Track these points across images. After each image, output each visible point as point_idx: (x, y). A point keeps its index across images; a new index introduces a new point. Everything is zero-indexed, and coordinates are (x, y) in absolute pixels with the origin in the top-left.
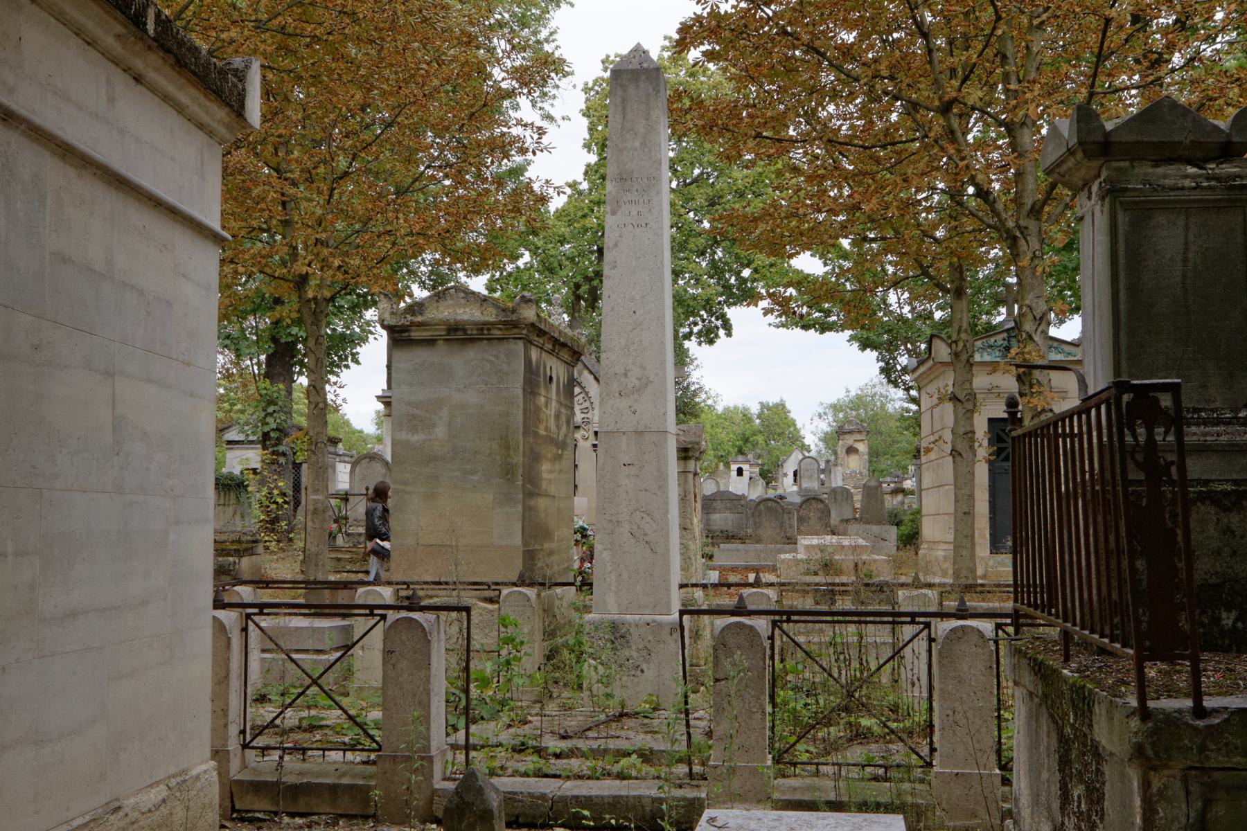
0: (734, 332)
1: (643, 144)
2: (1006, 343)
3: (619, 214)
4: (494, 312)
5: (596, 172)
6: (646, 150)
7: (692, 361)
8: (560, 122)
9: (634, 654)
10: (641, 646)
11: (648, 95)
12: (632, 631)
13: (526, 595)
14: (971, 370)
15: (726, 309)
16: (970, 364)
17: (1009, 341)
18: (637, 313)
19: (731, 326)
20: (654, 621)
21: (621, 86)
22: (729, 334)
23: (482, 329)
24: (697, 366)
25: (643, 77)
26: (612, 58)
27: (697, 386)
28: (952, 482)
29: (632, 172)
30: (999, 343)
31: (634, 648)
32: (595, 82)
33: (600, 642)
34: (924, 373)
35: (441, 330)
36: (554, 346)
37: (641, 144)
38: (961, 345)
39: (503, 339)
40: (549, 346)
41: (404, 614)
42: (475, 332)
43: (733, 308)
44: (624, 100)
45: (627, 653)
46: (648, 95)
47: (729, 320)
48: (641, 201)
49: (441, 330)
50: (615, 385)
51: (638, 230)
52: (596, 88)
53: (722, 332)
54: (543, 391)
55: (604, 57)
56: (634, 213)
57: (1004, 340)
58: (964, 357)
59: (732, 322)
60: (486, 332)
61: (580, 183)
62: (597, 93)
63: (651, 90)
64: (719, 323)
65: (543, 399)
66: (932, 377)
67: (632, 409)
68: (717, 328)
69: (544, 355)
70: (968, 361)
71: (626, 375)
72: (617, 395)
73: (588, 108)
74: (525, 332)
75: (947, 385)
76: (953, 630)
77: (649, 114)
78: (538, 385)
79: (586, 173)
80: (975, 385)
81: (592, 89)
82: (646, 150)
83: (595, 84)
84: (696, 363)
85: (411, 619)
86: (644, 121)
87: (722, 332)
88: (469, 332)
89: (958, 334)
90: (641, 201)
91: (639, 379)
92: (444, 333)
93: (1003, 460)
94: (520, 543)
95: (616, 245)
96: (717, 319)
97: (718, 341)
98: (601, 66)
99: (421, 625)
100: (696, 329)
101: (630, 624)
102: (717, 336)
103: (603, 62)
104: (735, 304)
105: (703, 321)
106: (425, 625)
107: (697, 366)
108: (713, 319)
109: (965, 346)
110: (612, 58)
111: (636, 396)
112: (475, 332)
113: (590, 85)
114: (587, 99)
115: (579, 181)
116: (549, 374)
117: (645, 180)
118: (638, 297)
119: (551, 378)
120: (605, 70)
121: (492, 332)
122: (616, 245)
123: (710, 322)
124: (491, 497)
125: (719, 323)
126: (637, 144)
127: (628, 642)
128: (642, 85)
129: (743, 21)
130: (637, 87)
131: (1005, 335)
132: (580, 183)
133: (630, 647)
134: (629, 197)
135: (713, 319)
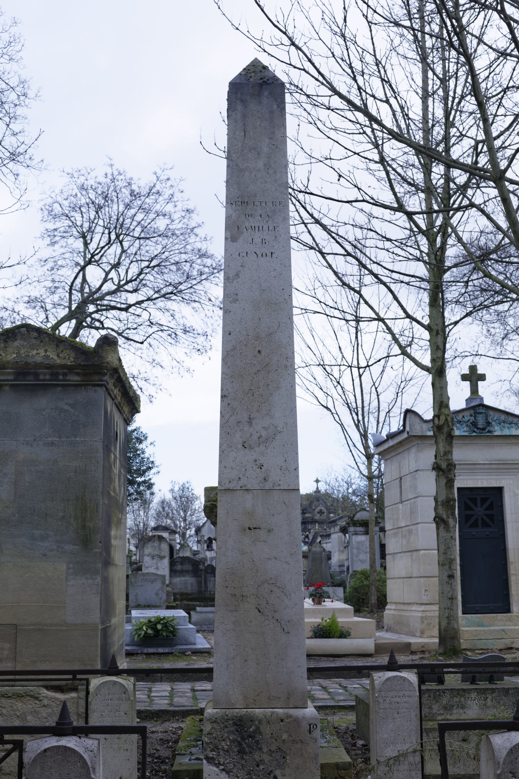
1: (267, 166)
2: (472, 418)
3: (240, 240)
4: (73, 355)
6: (271, 171)
9: (266, 758)
10: (274, 748)
12: (262, 729)
13: (122, 685)
14: (452, 442)
16: (450, 438)
17: (475, 417)
18: (263, 353)
20: (289, 716)
23: (57, 374)
28: (436, 548)
29: (255, 196)
30: (466, 419)
31: (265, 750)
33: (223, 743)
35: (9, 374)
39: (81, 385)
41: (52, 742)
42: (48, 377)
45: (257, 756)
46: (272, 112)
48: (266, 227)
49: (9, 374)
54: (113, 449)
56: (258, 240)
58: (445, 430)
60: (61, 377)
66: (401, 450)
72: (240, 446)
76: (388, 679)
77: (273, 133)
82: (271, 171)
84: (149, 441)
85: (66, 749)
88: (41, 377)
90: (266, 227)
92: (11, 377)
93: (471, 526)
94: (98, 621)
95: (237, 275)
99: (81, 757)
101: (260, 721)
106: (85, 756)
109: (446, 420)
111: (262, 448)
112: (48, 377)
117: (271, 204)
121: (68, 378)
122: (237, 275)
124: (64, 567)
126: (260, 164)
127: (257, 742)
128: (265, 101)
130: (260, 103)
133: (260, 749)
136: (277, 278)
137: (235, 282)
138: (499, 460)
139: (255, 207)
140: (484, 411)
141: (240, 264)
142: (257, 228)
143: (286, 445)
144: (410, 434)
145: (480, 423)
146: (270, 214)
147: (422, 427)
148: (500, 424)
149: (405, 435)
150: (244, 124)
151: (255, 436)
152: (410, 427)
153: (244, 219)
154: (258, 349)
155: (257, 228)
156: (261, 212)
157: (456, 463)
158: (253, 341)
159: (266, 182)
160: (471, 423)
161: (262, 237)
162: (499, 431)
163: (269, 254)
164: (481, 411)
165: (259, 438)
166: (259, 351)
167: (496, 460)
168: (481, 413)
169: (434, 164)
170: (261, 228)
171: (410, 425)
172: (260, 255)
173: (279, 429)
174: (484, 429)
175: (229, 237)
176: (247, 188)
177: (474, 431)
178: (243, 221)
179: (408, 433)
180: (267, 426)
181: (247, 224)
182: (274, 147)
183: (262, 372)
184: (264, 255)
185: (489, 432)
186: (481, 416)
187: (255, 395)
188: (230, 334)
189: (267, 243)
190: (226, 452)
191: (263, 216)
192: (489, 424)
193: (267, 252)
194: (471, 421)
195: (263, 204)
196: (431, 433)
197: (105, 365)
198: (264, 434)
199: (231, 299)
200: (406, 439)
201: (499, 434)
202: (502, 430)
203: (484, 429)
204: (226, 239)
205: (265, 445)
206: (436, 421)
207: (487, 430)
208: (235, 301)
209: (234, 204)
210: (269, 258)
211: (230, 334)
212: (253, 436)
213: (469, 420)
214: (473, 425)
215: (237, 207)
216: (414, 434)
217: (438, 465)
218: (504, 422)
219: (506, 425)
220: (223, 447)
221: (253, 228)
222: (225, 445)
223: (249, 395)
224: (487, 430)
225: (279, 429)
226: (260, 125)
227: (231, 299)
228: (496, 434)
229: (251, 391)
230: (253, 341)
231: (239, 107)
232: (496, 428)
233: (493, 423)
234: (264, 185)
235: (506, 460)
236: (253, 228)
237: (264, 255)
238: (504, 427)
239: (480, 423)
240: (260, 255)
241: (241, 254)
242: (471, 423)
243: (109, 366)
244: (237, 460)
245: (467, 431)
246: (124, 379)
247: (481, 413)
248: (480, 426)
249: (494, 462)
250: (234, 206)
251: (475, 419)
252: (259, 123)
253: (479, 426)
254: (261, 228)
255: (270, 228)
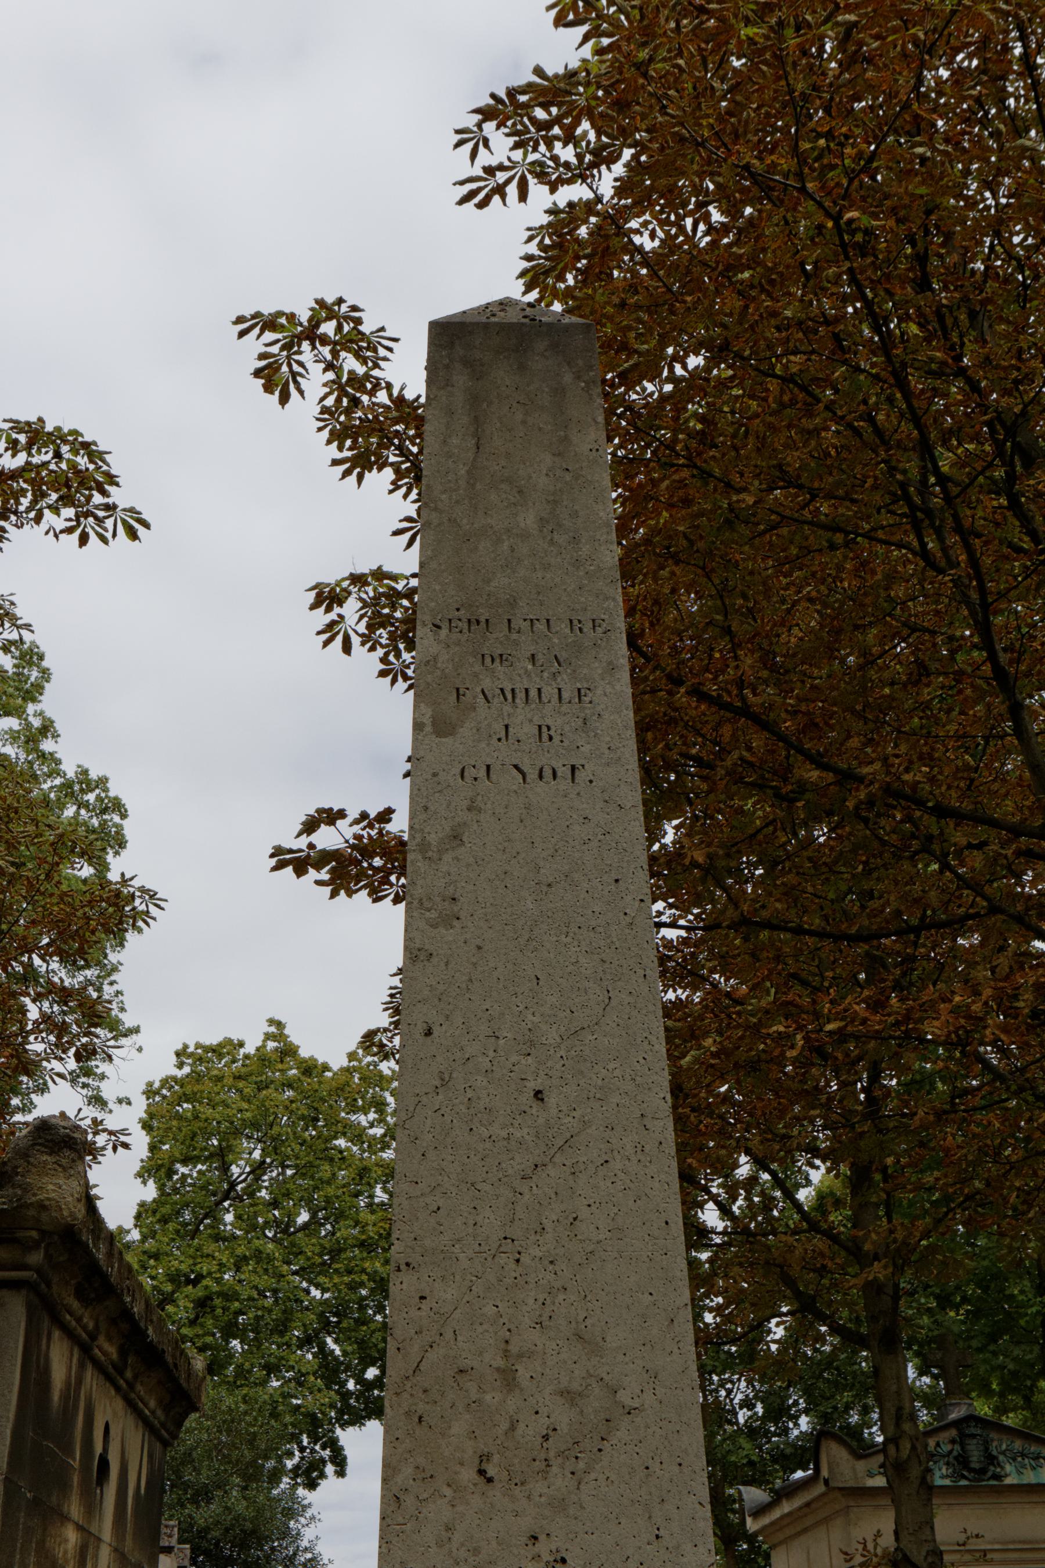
0: (349, 1470)
2: (957, 1447)
3: (466, 731)
5: (154, 1212)
6: (561, 539)
7: (305, 1508)
8: (111, 1105)
11: (559, 391)
14: (930, 1500)
15: (338, 1431)
18: (552, 1100)
19: (345, 1458)
21: (467, 363)
22: (341, 1473)
24: (313, 1518)
25: (541, 345)
26: (191, 1049)
27: (309, 1556)
29: (513, 603)
30: (946, 1448)
32: (165, 1082)
34: (790, 1514)
36: (123, 1352)
37: (542, 521)
38: (906, 1446)
40: (108, 1349)
43: (350, 1430)
44: (474, 400)
46: (559, 391)
47: (342, 1448)
48: (549, 692)
50: (458, 1428)
51: (541, 791)
52: (164, 1092)
53: (330, 1469)
54: (75, 1509)
55: (180, 1047)
56: (524, 730)
57: (953, 1442)
58: (915, 1472)
59: (346, 1452)
61: (128, 1232)
62: (164, 1097)
63: (568, 378)
64: (327, 1453)
65: (72, 1536)
66: (809, 1521)
67: (542, 1537)
68: (323, 1462)
69: (91, 1378)
70: (923, 1480)
71: (508, 1379)
72: (468, 1475)
73: (151, 1115)
74: (36, 1258)
75: (878, 1534)
78: (64, 1487)
79: (138, 1217)
80: (939, 1538)
81: (157, 1092)
83: (162, 1087)
84: (309, 1513)
86: (548, 459)
87: (330, 1469)
89: (898, 1425)
90: (549, 692)
91: (569, 1396)
95: (456, 837)
96: (323, 1448)
97: (323, 1484)
98: (174, 1059)
100: (289, 1464)
102: (322, 1475)
103: (178, 1054)
104: (352, 1423)
105: (302, 1449)
107: (313, 1518)
108: (317, 1448)
109: (914, 1448)
110: (191, 1049)
111: (560, 1481)
113: (157, 1085)
114: (149, 1105)
115: (126, 1227)
116: (99, 1449)
118: (552, 1036)
119: (104, 1464)
120: (180, 1066)
122: (456, 837)
123: (313, 1451)
125: (327, 1453)
126: (528, 519)
129: (681, 493)
130: (522, 368)
131: (953, 1432)
132: (128, 1232)
134: (502, 677)
135: (317, 1448)
136: (594, 844)
137: (447, 857)
138: (1020, 1542)
139: (514, 636)
140: (979, 1432)
141: (466, 803)
142: (521, 695)
143: (655, 1467)
144: (832, 1484)
145: (974, 1459)
146: (563, 655)
147: (854, 1469)
148: (1014, 1460)
149: (821, 1488)
150: (476, 419)
151: (530, 1430)
152: (831, 1470)
153: (478, 668)
154: (532, 1085)
155: (521, 695)
156: (532, 649)
157: (942, 1548)
158: (514, 1058)
159: (546, 567)
160: (956, 1458)
161: (537, 721)
162: (1014, 1475)
163: (564, 772)
164: (973, 1431)
165: (546, 1438)
166: (538, 1095)
167: (1013, 1542)
168: (974, 1436)
169: (700, 1214)
170: (533, 693)
171: (829, 1463)
172: (532, 775)
173: (623, 1396)
174: (982, 1471)
175: (427, 720)
176: (489, 581)
177: (964, 1477)
178: (476, 675)
179: (826, 1482)
180: (575, 1386)
181: (487, 683)
182: (568, 477)
183: (551, 1170)
184: (548, 773)
185: (997, 1477)
186: (975, 1441)
187: (525, 1259)
188: (429, 1033)
189: (556, 739)
190: (409, 1501)
191: (540, 659)
192: (991, 1459)
193: (557, 764)
194: (955, 1453)
195: (541, 627)
196: (880, 1481)
197: (32, 1212)
198: (563, 1417)
199: (433, 914)
200: (823, 1495)
201: (1015, 1482)
202: (1020, 1473)
203: (982, 1471)
204: (418, 726)
205: (570, 1465)
206: (892, 1450)
207: (990, 1474)
208: (449, 920)
209: (445, 625)
210: (564, 784)
211: (429, 1033)
212: (521, 1428)
213: (951, 1452)
214: (959, 1463)
215: (455, 636)
216: (841, 1485)
217: (905, 1555)
218: (1023, 1455)
219: (1026, 1461)
220: (399, 1479)
221: (508, 695)
222: (408, 1471)
223: (502, 1259)
224: (990, 1474)
225: (623, 1396)
226: (524, 422)
227: (433, 914)
228: (1008, 1481)
229: (508, 1246)
230: (514, 1058)
231: (461, 379)
232: (1008, 1468)
233: (1001, 1458)
234: (540, 575)
235: (1037, 1542)
236: (508, 695)
237: (548, 773)
238: (1024, 1466)
239: (974, 1459)
240: (532, 775)
241: (470, 773)
242: (956, 1458)
243: (44, 1217)
244: (457, 1537)
245: (947, 1476)
246: (113, 1272)
247: (974, 1436)
248: (975, 1465)
249: (1011, 1547)
250: (444, 632)
251: (963, 1448)
252: (519, 416)
253: (973, 1465)
254: (533, 693)
255: (566, 695)
